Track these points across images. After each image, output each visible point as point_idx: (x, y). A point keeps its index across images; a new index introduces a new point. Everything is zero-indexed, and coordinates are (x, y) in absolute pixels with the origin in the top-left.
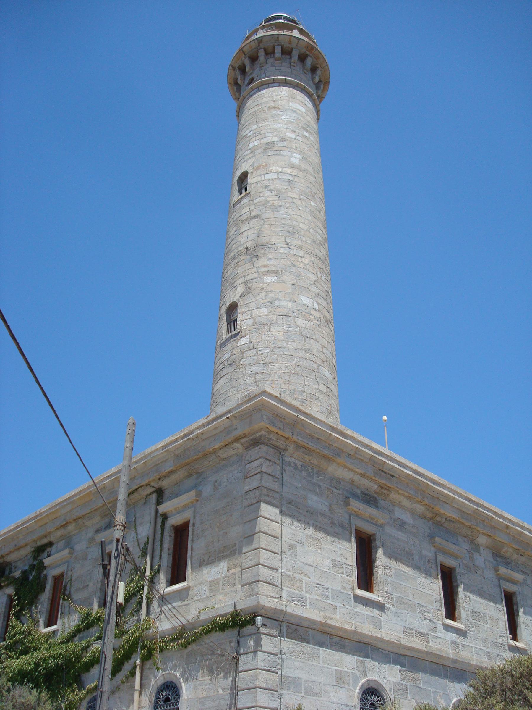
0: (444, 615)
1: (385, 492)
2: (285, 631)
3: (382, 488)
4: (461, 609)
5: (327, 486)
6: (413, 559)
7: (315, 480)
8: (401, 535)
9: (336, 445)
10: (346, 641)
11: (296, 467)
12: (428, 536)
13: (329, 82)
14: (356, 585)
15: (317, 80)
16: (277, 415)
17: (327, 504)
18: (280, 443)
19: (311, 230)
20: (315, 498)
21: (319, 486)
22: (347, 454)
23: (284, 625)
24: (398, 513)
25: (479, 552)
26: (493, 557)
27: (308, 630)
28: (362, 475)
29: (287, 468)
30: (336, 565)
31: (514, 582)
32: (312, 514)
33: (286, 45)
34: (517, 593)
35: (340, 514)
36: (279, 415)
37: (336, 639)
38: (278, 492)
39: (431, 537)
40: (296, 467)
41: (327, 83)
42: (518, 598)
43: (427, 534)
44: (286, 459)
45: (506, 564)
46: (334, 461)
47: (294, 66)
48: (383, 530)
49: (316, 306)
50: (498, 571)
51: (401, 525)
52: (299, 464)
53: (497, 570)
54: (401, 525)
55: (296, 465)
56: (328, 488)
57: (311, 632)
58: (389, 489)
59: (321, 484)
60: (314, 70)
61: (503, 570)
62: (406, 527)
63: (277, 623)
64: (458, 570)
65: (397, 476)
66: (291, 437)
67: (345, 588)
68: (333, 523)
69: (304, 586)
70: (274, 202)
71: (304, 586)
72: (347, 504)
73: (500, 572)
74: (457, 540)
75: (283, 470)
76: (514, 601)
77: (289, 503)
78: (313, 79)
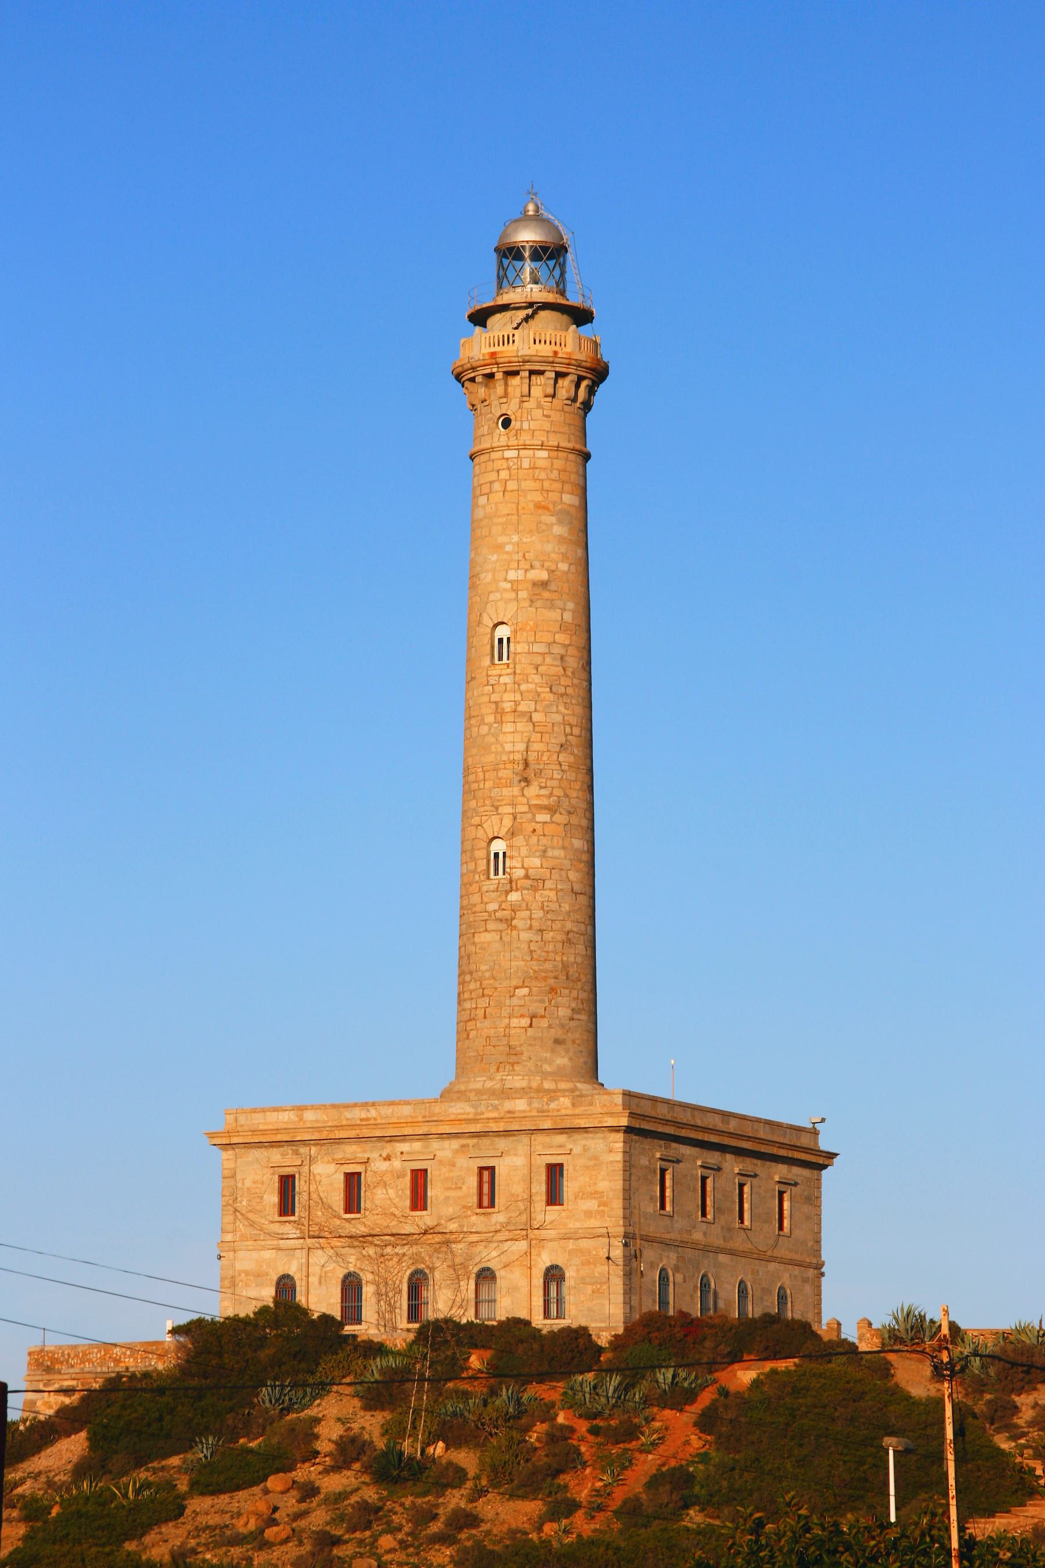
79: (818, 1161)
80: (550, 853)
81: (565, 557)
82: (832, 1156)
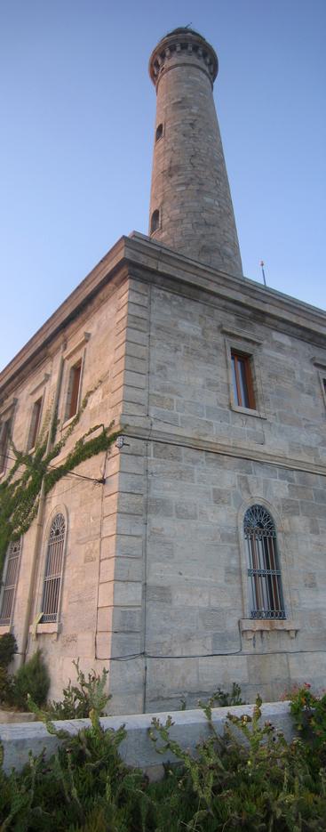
20: (186, 323)
30: (210, 384)
49: (217, 203)
67: (221, 405)
69: (175, 404)
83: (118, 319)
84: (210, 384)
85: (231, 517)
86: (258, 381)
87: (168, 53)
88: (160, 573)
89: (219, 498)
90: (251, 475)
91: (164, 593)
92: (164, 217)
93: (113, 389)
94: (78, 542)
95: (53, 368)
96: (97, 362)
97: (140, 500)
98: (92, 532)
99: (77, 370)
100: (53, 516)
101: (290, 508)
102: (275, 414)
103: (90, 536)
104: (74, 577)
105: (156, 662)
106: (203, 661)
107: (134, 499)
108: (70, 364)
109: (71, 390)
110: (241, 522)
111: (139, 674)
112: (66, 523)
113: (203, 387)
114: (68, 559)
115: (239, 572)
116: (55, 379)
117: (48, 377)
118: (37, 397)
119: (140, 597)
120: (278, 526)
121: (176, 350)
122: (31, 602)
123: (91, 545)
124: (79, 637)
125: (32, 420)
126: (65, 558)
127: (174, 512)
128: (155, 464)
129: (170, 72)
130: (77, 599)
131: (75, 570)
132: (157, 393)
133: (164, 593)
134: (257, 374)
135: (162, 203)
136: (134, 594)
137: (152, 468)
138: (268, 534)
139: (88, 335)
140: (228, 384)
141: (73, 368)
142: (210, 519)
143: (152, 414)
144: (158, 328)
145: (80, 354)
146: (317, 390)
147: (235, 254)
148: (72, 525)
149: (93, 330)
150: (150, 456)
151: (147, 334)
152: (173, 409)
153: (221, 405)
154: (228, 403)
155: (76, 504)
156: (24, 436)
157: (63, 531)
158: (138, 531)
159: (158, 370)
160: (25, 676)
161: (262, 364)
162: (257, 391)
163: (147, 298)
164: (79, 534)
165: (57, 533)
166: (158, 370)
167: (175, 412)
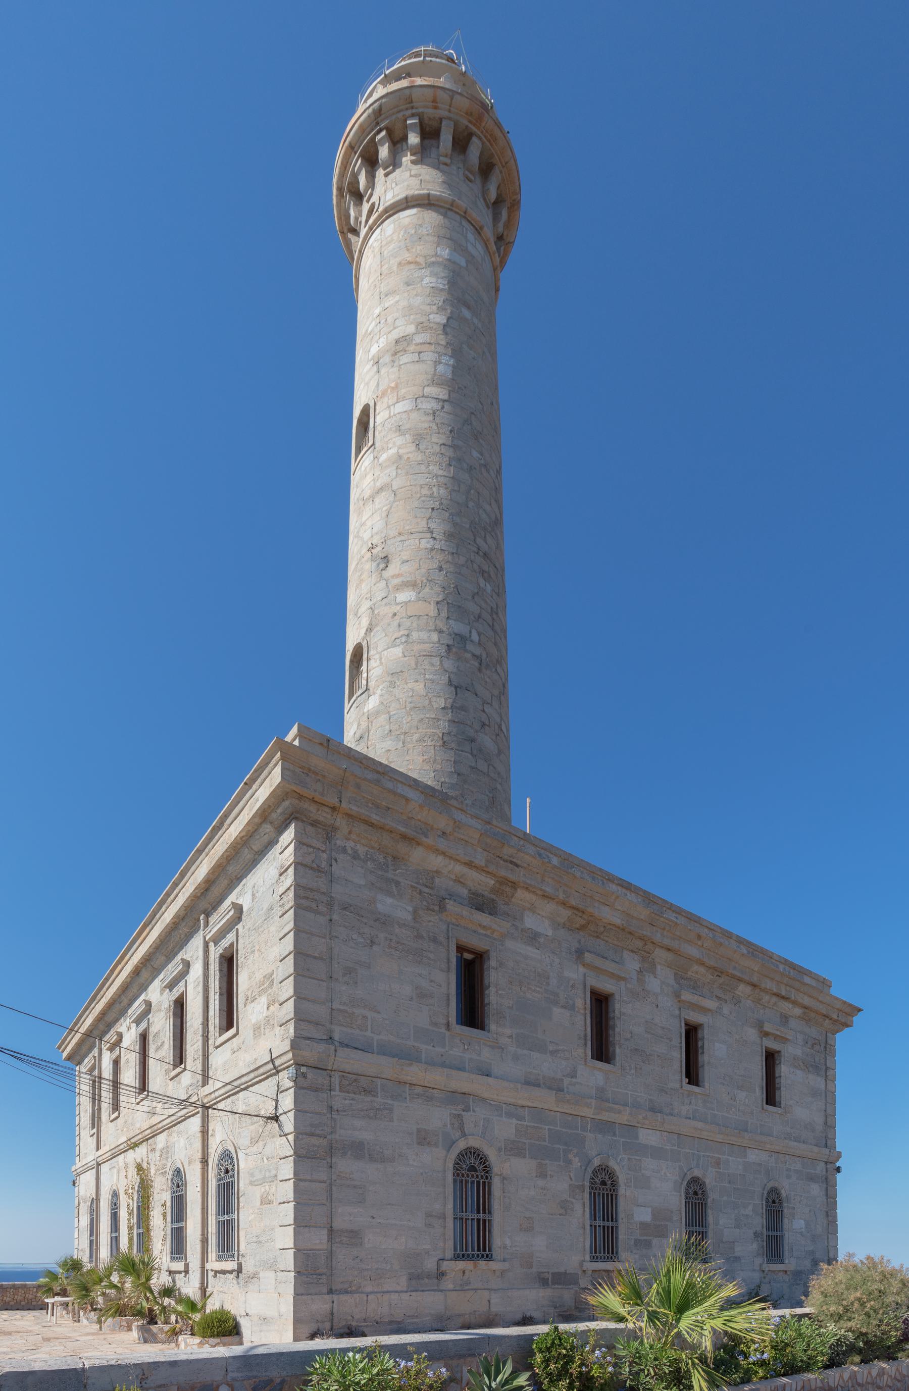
0: (589, 1053)
1: (508, 889)
2: (337, 1083)
3: (501, 883)
4: (617, 1047)
5: (410, 883)
6: (548, 984)
7: (390, 875)
8: (531, 951)
9: (419, 817)
10: (435, 1091)
11: (355, 856)
12: (576, 952)
13: (519, 202)
14: (453, 1019)
15: (493, 195)
16: (310, 770)
17: (411, 909)
18: (324, 816)
19: (471, 504)
20: (389, 900)
21: (397, 883)
22: (440, 833)
23: (337, 1075)
24: (530, 921)
25: (654, 973)
26: (675, 979)
27: (374, 1079)
28: (469, 865)
29: (341, 857)
30: (422, 995)
31: (705, 1010)
32: (384, 923)
33: (430, 112)
34: (706, 1026)
35: (431, 924)
36: (313, 768)
37: (419, 1090)
38: (324, 893)
39: (579, 954)
40: (355, 856)
41: (515, 205)
42: (706, 1031)
43: (573, 949)
44: (339, 842)
45: (694, 988)
46: (418, 844)
47: (446, 164)
48: (503, 945)
49: (475, 637)
50: (762, 1027)
51: (533, 938)
52: (362, 850)
53: (677, 995)
54: (533, 938)
55: (356, 852)
56: (412, 886)
57: (379, 1081)
58: (514, 885)
59: (400, 880)
60: (486, 169)
61: (686, 996)
62: (542, 940)
63: (325, 1073)
64: (617, 997)
65: (525, 865)
66: (337, 805)
67: (435, 1024)
68: (419, 937)
69: (369, 1023)
70: (409, 455)
71: (369, 1023)
72: (442, 908)
73: (683, 997)
74: (622, 957)
75: (332, 861)
76: (700, 1036)
77: (345, 909)
78: (485, 193)
79: (844, 1015)
80: (415, 635)
81: (441, 309)
82: (860, 1010)
83: (282, 890)
84: (422, 995)
85: (439, 1162)
86: (492, 990)
87: (384, 152)
88: (348, 1216)
89: (423, 1139)
90: (469, 1113)
91: (354, 1236)
92: (372, 663)
93: (282, 999)
94: (252, 1183)
95: (193, 950)
96: (257, 954)
97: (324, 1142)
98: (267, 1174)
99: (229, 962)
100: (219, 1151)
101: (514, 1149)
102: (511, 1037)
103: (264, 1178)
104: (250, 1218)
105: (344, 1297)
106: (394, 1296)
107: (314, 1141)
108: (215, 953)
109: (225, 990)
110: (451, 1166)
111: (327, 1307)
112: (235, 1161)
113: (411, 999)
114: (241, 1199)
115: (443, 1217)
116: (196, 971)
117: (187, 965)
118: (176, 993)
119: (325, 1241)
120: (496, 1169)
121: (372, 943)
122: (204, 1241)
123: (267, 1187)
124: (261, 1275)
125: (174, 1025)
126: (238, 1198)
127: (367, 1155)
128: (340, 1100)
129: (389, 227)
130: (255, 1239)
131: (251, 1211)
132: (342, 1007)
133: (354, 1236)
134: (492, 979)
135: (370, 630)
136: (319, 1239)
137: (338, 1103)
138: (482, 1177)
139: (238, 909)
140: (448, 995)
141: (222, 956)
142: (411, 1162)
143: (336, 1037)
144: (345, 907)
145: (230, 937)
146: (579, 1003)
147: (500, 752)
148: (245, 1164)
149: (246, 902)
150: (335, 1090)
151: (328, 917)
152: (367, 1030)
153: (435, 1024)
154: (445, 1021)
155: (247, 1142)
156: (166, 1046)
157: (233, 1170)
158: (323, 1176)
159: (344, 975)
160: (458, 1164)
161: (501, 964)
162: (489, 1004)
163: (325, 856)
164: (252, 1175)
165: (227, 1171)
166: (344, 975)
167: (369, 1034)
